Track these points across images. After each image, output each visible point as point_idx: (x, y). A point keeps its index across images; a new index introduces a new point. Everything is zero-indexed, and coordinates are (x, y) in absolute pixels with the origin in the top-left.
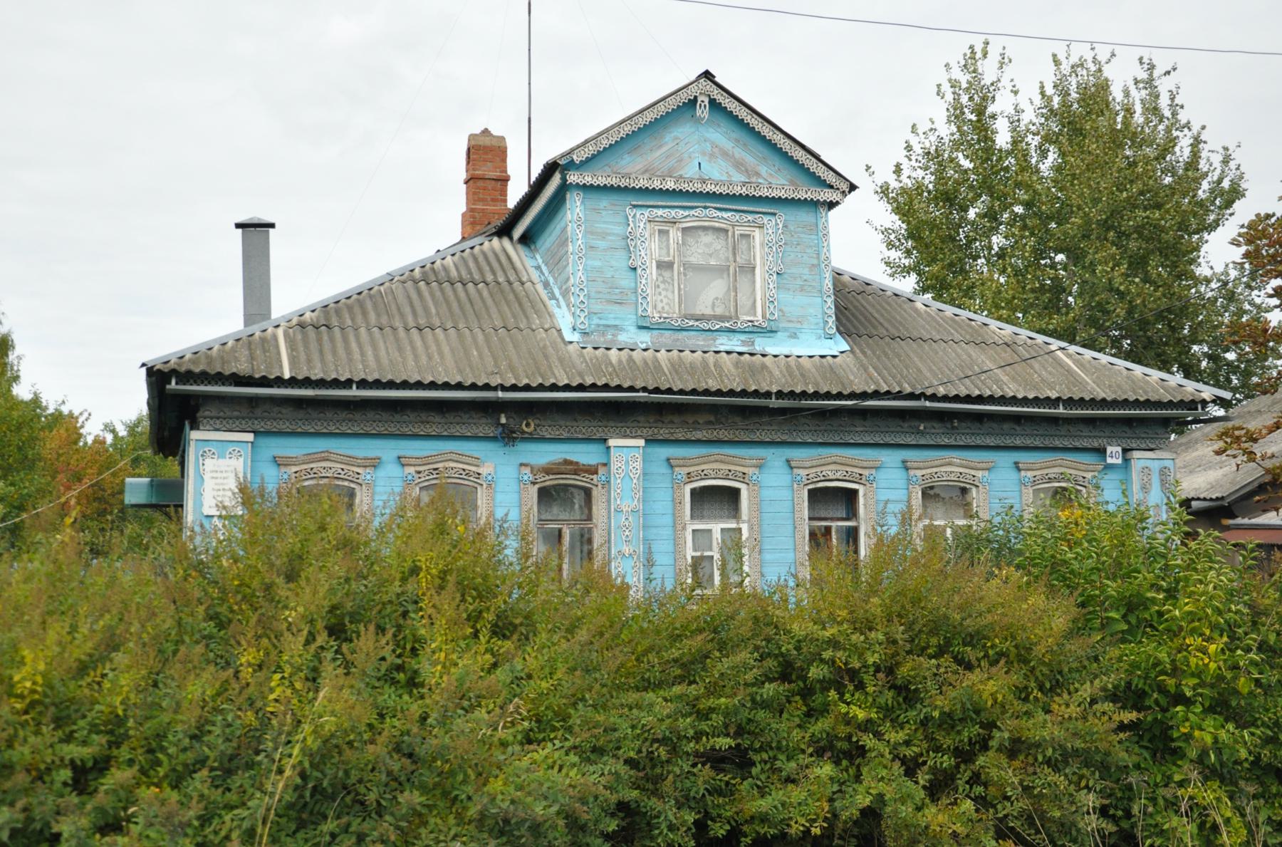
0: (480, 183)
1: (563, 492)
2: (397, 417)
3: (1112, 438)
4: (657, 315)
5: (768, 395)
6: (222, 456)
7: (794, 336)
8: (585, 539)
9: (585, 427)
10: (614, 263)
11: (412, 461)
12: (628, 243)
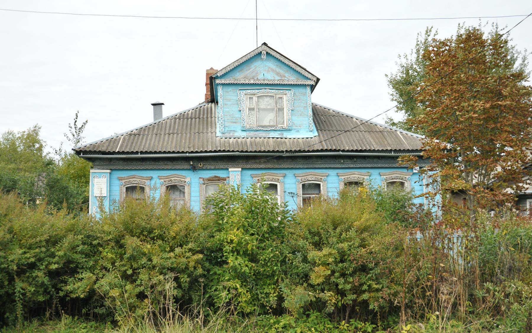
2: (157, 163)
4: (248, 126)
5: (282, 152)
7: (298, 131)
9: (221, 165)
10: (233, 109)
11: (162, 178)
12: (238, 102)
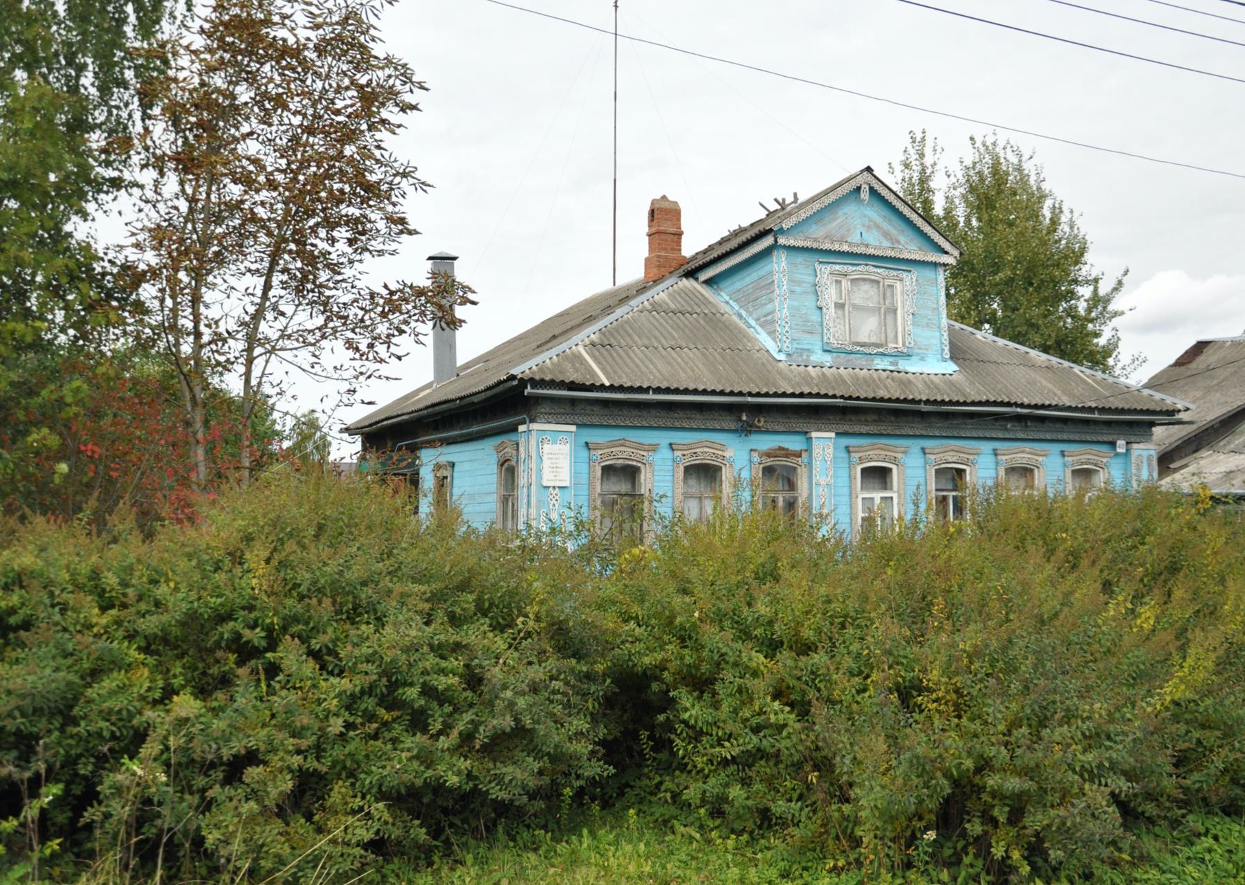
0: (663, 236)
1: (780, 473)
2: (672, 414)
3: (1121, 435)
5: (919, 402)
6: (555, 442)
7: (923, 359)
8: (791, 505)
9: (798, 424)
12: (815, 290)
